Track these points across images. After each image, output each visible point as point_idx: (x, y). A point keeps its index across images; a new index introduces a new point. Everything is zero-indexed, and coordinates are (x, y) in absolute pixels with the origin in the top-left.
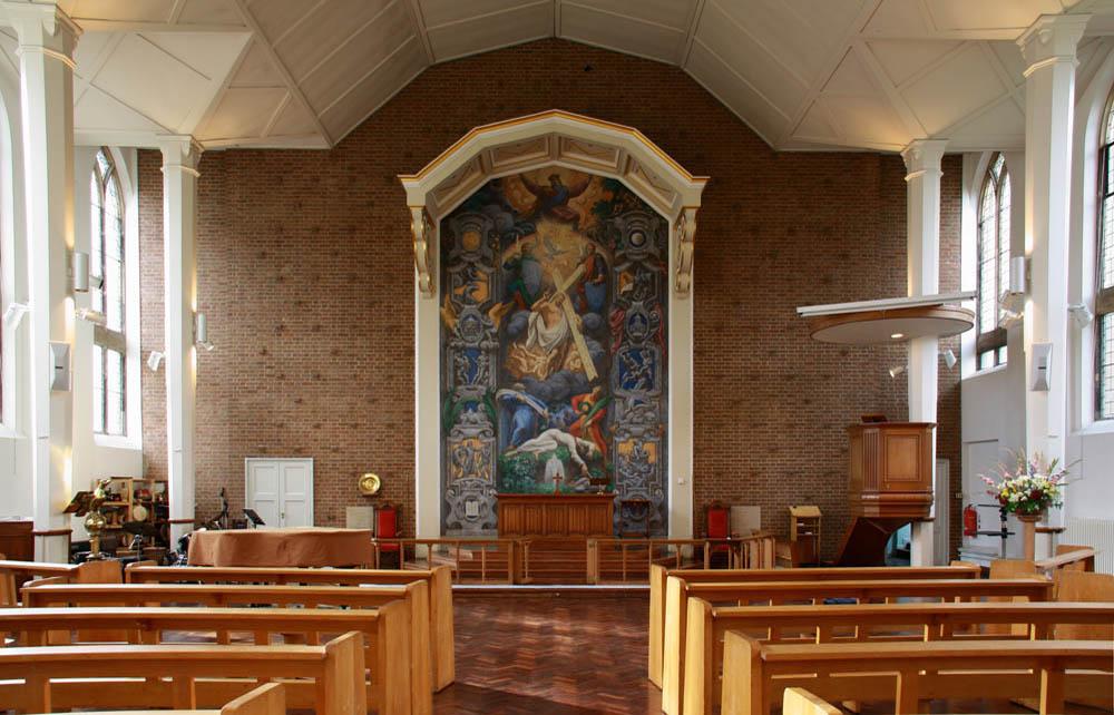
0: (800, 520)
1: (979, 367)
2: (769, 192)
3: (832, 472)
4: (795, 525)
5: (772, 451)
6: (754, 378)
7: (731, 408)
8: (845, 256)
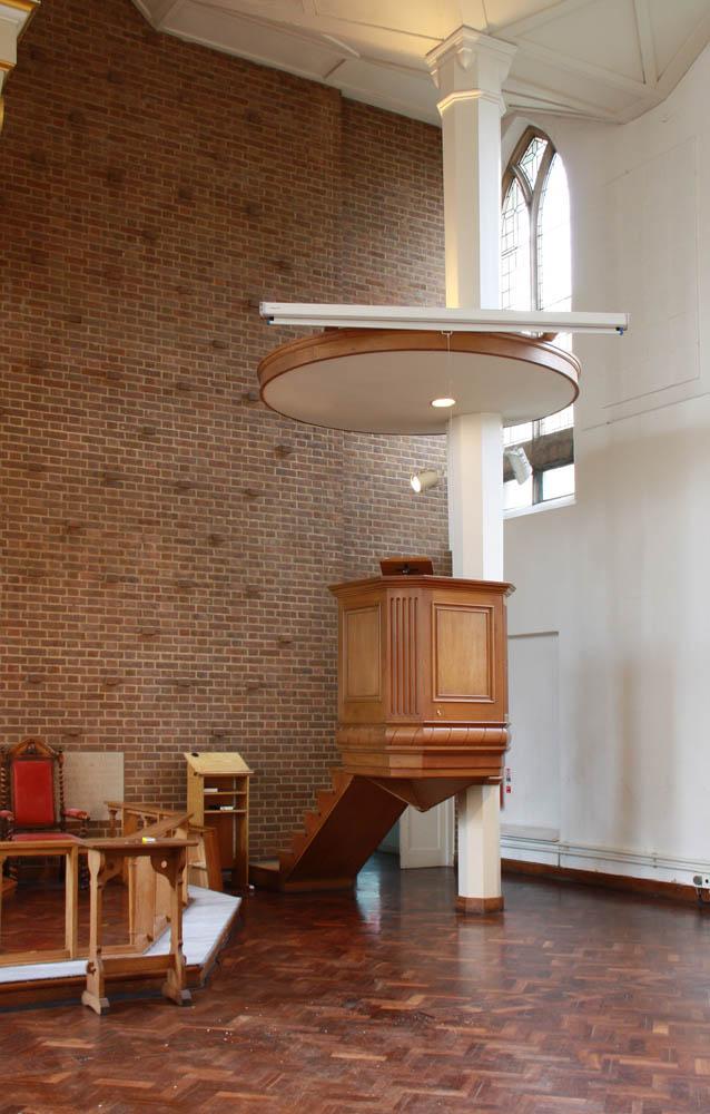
0: (210, 780)
1: (538, 498)
2: (143, 106)
3: (262, 686)
4: (196, 795)
5: (147, 636)
6: (110, 480)
7: (62, 539)
8: (282, 266)
